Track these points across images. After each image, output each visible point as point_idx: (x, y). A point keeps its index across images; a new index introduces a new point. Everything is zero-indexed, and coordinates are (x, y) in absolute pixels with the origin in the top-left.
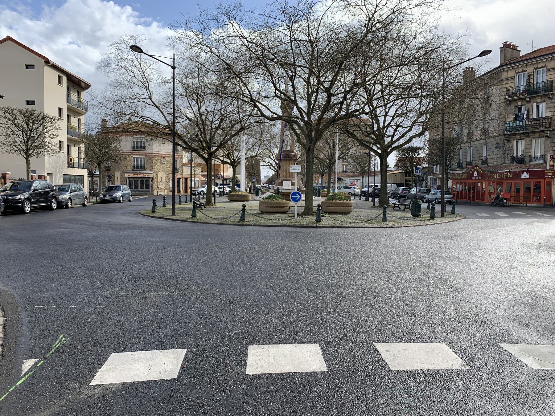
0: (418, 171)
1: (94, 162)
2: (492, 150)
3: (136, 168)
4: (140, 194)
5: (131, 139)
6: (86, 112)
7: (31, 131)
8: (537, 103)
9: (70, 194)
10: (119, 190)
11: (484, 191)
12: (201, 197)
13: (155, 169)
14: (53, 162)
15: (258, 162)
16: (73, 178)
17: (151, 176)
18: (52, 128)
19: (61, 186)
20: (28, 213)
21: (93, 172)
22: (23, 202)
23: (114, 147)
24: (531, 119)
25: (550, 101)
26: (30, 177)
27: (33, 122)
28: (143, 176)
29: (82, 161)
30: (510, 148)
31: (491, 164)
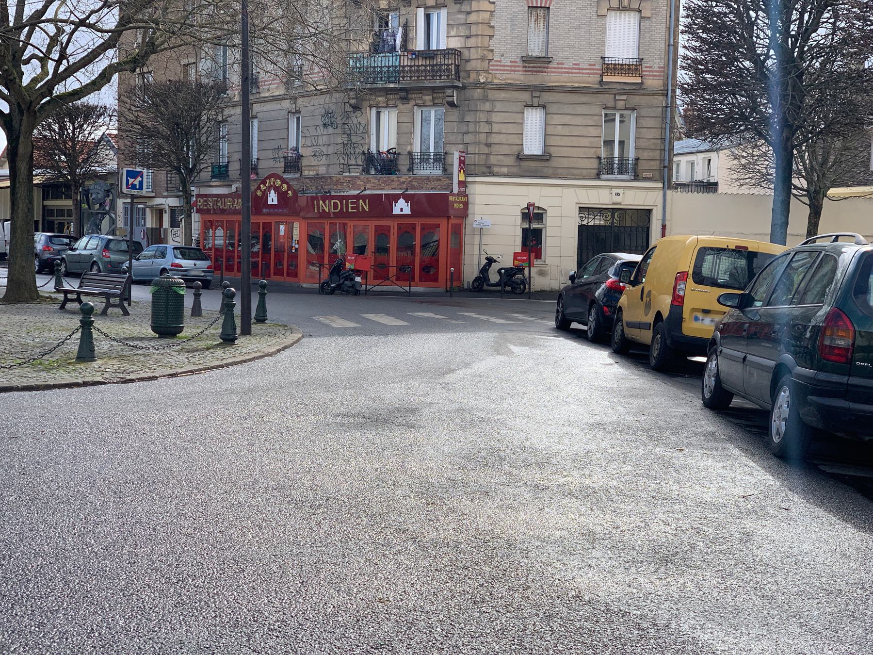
0: (137, 182)
2: (313, 132)
8: (426, 8)
11: (296, 249)
24: (413, 52)
25: (459, 6)
30: (361, 128)
31: (311, 173)
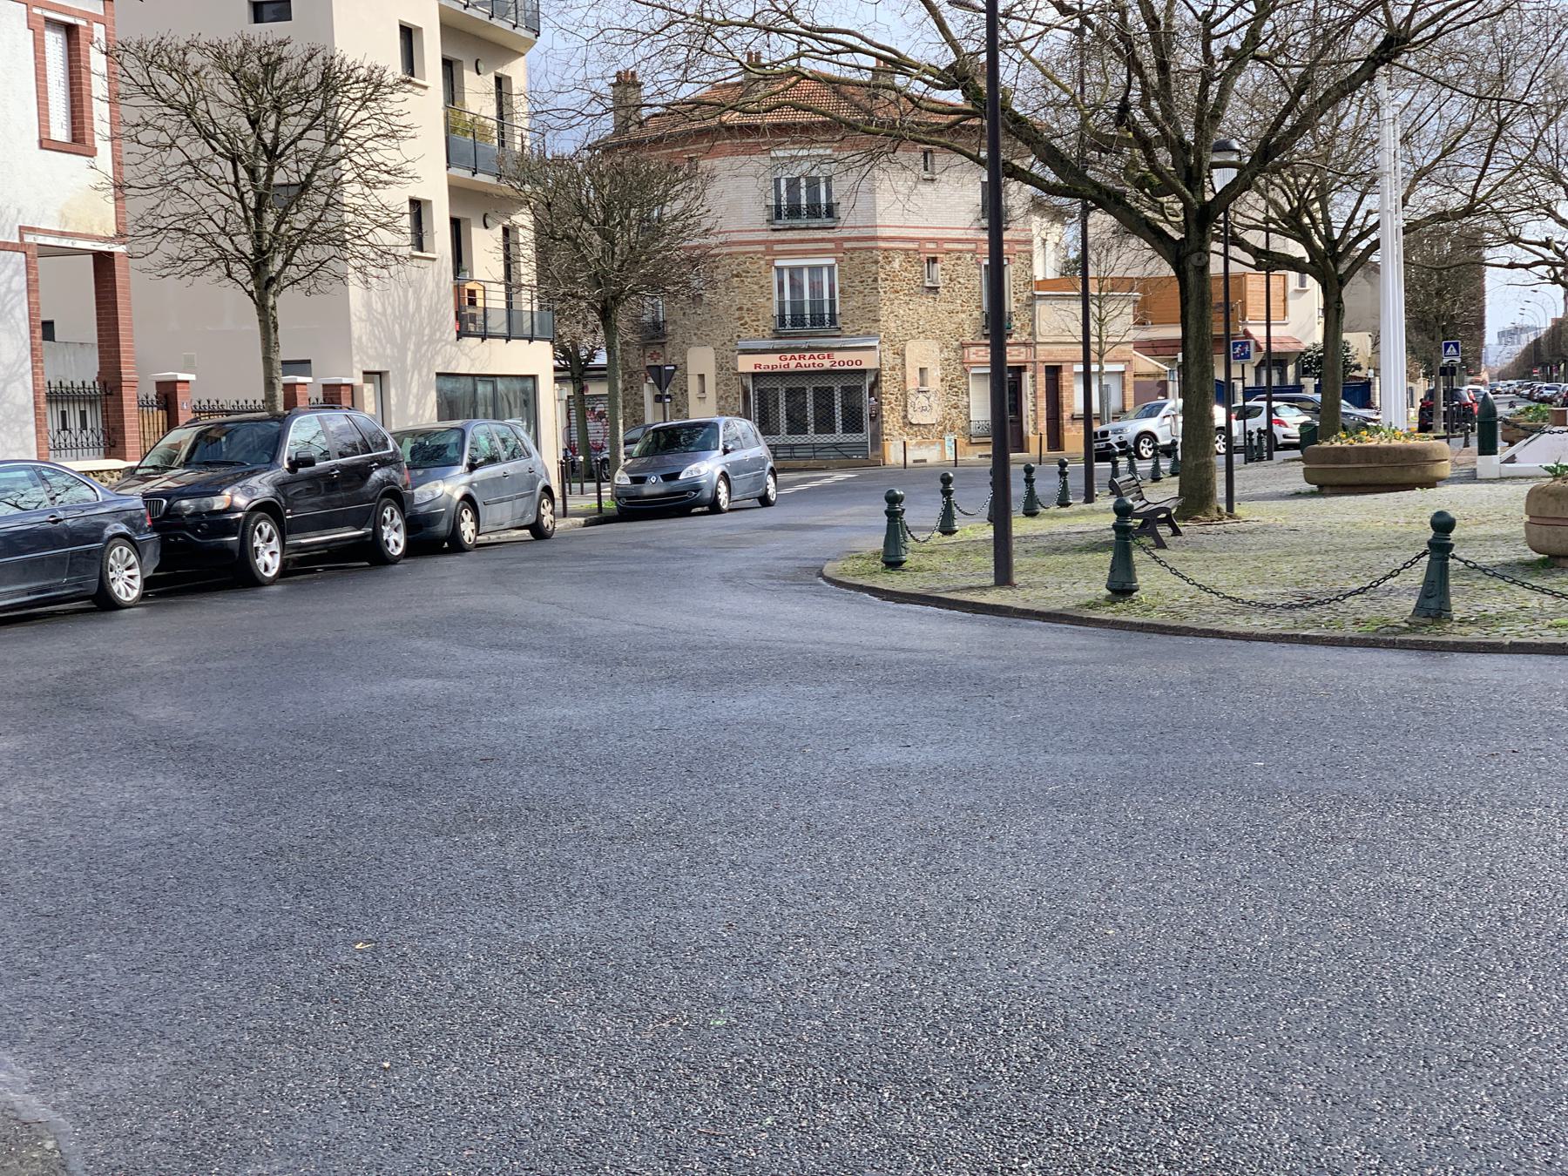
1: (584, 304)
3: (794, 324)
4: (818, 460)
5: (755, 164)
6: (532, 35)
7: (272, 154)
9: (467, 478)
10: (706, 447)
12: (1144, 466)
13: (889, 324)
14: (389, 311)
15: (1474, 242)
16: (483, 389)
17: (868, 361)
18: (367, 132)
19: (427, 434)
20: (273, 581)
21: (583, 354)
22: (243, 528)
23: (675, 219)
26: (280, 394)
27: (278, 108)
28: (827, 364)
29: (527, 303)
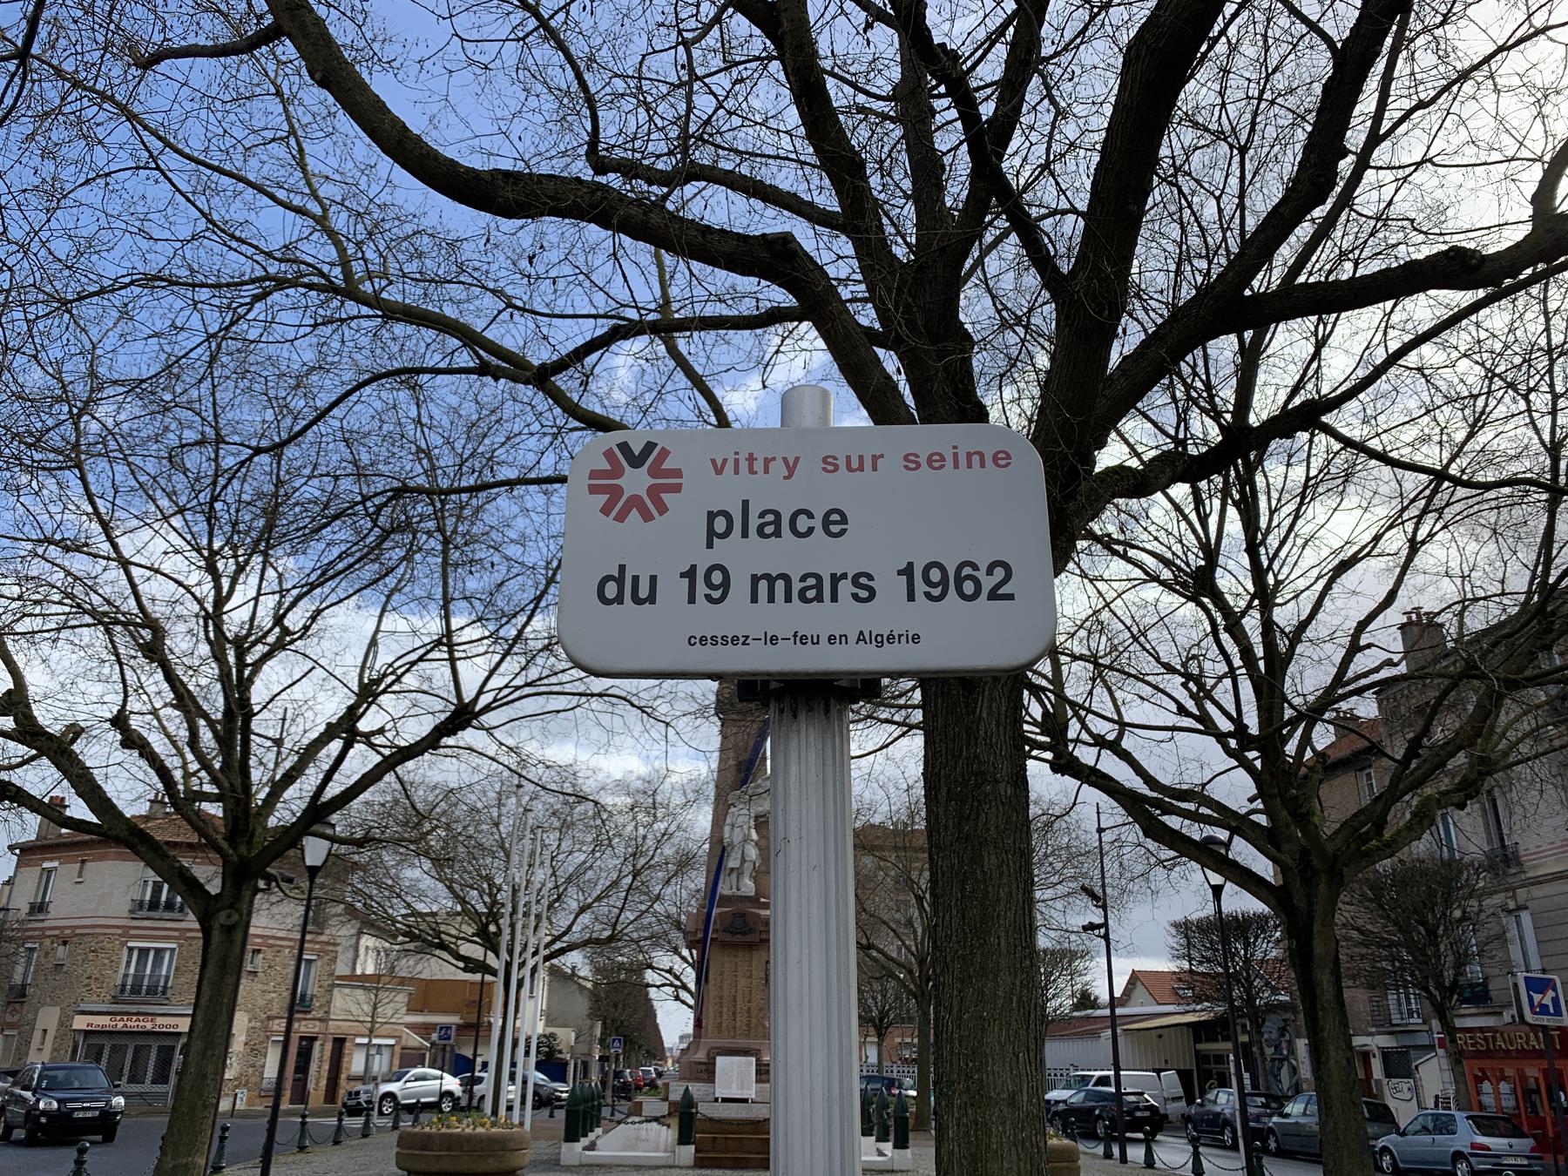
0: (1547, 1001)
28: (149, 1026)
